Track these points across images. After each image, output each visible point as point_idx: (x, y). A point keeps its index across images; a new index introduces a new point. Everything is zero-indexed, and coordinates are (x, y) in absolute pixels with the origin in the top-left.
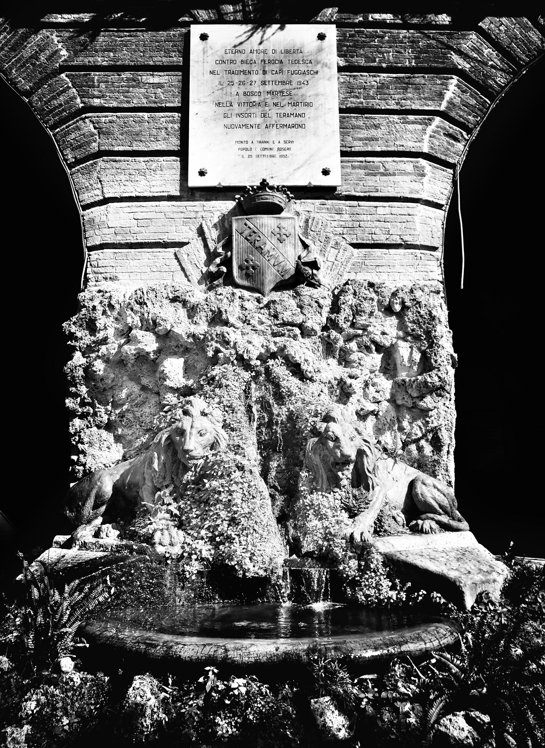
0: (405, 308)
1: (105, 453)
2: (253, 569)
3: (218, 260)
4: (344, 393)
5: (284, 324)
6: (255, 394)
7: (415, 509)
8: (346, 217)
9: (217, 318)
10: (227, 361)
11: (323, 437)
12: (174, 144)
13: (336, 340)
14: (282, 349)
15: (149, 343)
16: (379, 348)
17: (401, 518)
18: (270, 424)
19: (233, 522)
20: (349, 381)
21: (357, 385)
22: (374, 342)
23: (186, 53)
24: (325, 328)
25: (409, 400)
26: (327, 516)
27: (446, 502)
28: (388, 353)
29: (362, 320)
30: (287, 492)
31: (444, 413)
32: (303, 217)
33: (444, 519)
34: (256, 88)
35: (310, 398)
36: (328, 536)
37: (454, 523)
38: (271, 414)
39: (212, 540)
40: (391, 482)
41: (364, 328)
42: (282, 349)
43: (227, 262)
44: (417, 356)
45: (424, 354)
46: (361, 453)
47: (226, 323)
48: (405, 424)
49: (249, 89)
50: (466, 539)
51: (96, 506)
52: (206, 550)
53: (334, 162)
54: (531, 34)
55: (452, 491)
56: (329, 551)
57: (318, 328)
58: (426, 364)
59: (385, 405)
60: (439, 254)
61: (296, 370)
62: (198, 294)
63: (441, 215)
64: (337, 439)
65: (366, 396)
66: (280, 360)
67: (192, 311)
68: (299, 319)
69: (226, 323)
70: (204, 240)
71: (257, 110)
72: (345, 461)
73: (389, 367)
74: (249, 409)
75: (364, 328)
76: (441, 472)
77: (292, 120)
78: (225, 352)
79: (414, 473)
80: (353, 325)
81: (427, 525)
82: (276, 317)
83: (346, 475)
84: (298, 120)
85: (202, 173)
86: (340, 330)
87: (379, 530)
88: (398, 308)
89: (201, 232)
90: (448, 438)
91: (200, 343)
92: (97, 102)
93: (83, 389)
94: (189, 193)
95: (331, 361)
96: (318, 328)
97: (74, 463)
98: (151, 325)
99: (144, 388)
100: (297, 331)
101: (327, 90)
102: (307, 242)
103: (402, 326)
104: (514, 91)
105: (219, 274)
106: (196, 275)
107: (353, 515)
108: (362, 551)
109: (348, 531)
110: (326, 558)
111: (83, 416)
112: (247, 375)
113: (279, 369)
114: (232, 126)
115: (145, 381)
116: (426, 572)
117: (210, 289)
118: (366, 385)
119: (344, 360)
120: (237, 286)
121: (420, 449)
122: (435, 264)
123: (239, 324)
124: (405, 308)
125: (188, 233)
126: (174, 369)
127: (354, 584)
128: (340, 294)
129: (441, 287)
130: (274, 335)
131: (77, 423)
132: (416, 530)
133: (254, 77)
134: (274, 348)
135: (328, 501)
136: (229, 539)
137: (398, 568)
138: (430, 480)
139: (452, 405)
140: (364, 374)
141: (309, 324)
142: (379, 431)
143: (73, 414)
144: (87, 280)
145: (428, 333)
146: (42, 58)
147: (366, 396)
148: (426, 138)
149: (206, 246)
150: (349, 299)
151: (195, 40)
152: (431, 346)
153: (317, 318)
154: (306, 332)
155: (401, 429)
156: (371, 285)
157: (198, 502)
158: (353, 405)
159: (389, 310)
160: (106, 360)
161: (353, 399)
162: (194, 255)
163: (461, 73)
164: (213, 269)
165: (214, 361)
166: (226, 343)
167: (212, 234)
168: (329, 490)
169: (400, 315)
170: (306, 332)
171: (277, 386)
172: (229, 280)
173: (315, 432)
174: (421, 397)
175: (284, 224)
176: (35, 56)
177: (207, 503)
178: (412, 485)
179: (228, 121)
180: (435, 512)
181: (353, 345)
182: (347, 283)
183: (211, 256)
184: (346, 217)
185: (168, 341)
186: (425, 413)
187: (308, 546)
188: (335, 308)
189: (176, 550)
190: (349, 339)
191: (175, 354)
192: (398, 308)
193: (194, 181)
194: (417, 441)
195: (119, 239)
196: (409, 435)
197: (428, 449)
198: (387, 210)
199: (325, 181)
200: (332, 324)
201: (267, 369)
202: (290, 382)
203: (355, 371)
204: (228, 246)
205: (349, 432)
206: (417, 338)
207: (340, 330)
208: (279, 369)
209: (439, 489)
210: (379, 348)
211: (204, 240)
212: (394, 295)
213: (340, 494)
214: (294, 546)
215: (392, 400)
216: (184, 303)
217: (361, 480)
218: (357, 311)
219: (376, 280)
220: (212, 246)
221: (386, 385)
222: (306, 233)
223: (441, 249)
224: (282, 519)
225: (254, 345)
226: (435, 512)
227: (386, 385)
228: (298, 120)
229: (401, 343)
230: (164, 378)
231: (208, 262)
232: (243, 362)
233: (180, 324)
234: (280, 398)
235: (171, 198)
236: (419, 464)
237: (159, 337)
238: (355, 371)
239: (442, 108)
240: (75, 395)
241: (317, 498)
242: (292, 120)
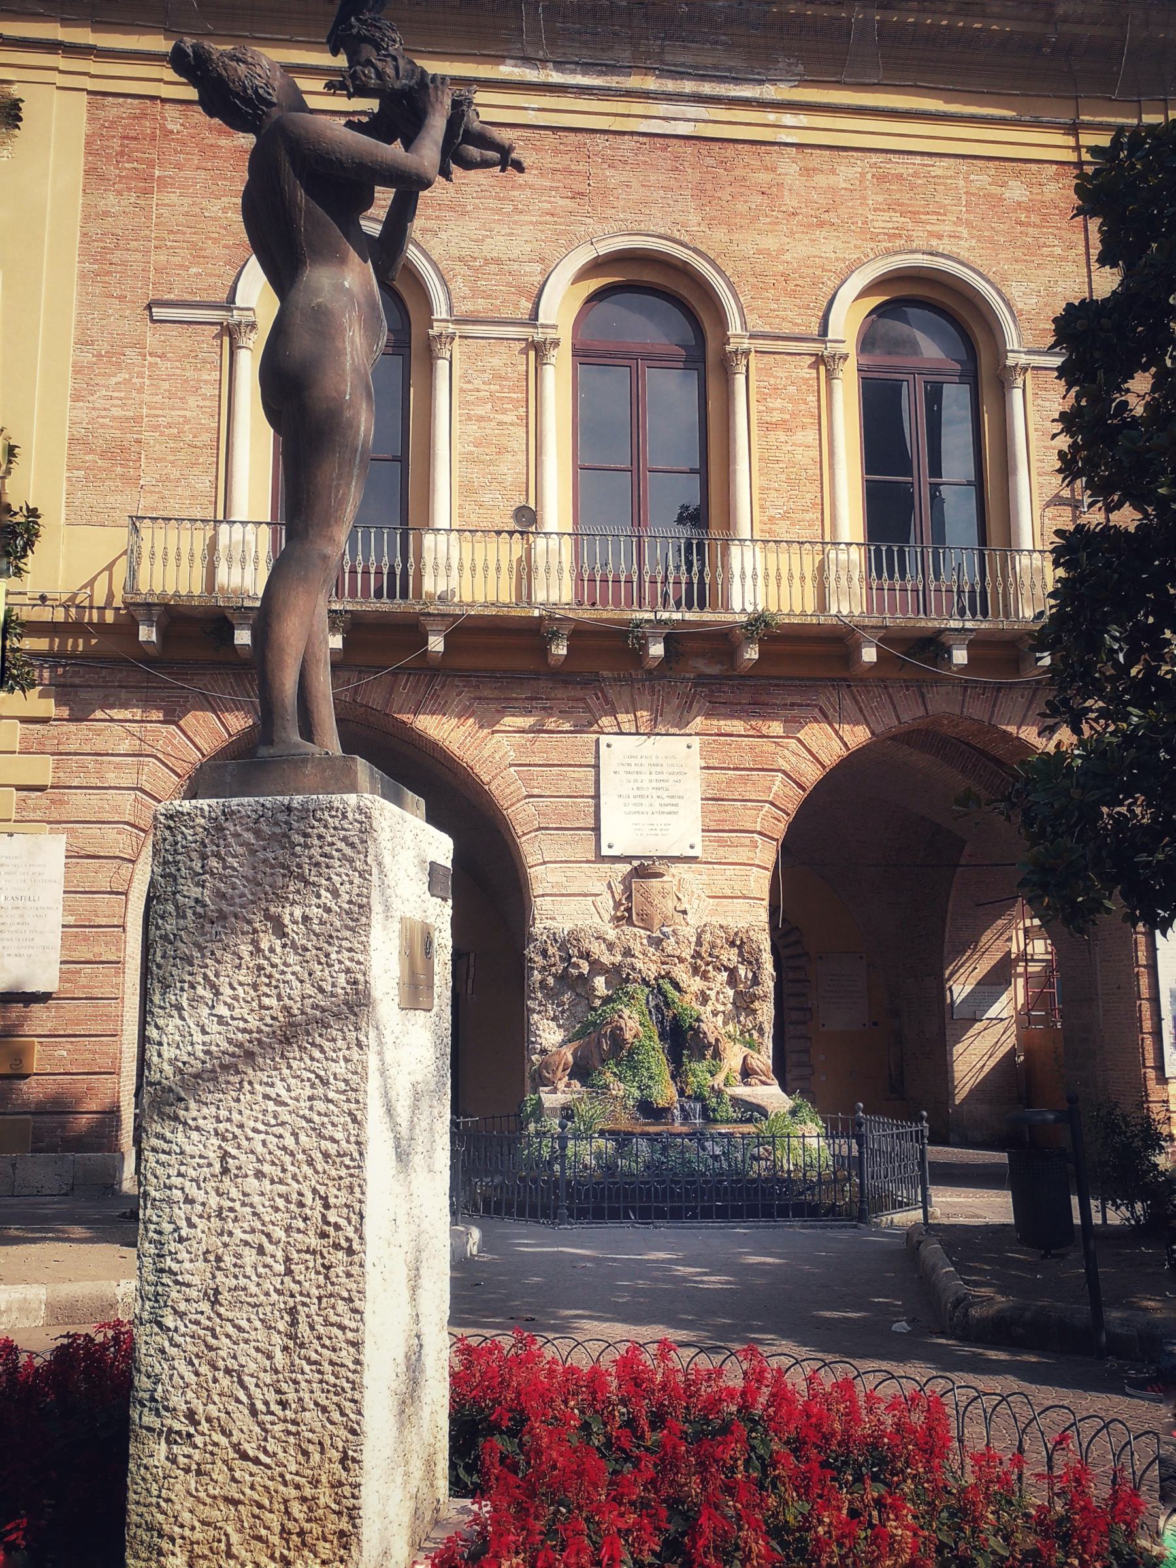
0: (742, 942)
1: (552, 1036)
2: (662, 1103)
3: (622, 908)
4: (704, 999)
5: (668, 956)
6: (652, 1004)
7: (747, 1073)
8: (704, 877)
9: (628, 953)
10: (635, 981)
11: (697, 1031)
12: (591, 823)
13: (700, 966)
14: (668, 973)
15: (585, 967)
16: (726, 969)
17: (739, 1078)
18: (662, 1022)
19: (651, 1078)
20: (708, 992)
21: (712, 994)
22: (723, 965)
23: (597, 757)
24: (693, 957)
25: (744, 1003)
26: (698, 1071)
27: (764, 1068)
28: (732, 972)
29: (716, 952)
30: (675, 1059)
31: (766, 1012)
32: (677, 878)
33: (763, 1078)
34: (644, 785)
35: (688, 1003)
36: (700, 1086)
37: (769, 1081)
38: (663, 1014)
39: (639, 1088)
40: (734, 1056)
41: (717, 957)
42: (668, 973)
43: (629, 910)
44: (750, 975)
45: (754, 973)
46: (717, 1040)
47: (633, 956)
48: (742, 1019)
49: (639, 785)
50: (775, 1089)
51: (564, 1070)
52: (637, 1094)
53: (697, 838)
54: (833, 742)
55: (770, 1062)
56: (701, 1094)
57: (688, 957)
58: (756, 981)
59: (730, 1006)
60: (766, 903)
61: (676, 986)
62: (612, 934)
63: (769, 874)
64: (705, 1033)
65: (717, 1000)
66: (667, 980)
67: (610, 946)
68: (677, 953)
69: (633, 956)
70: (612, 892)
71: (645, 801)
72: (710, 1044)
73: (733, 980)
74: (650, 1012)
75: (717, 957)
76: (763, 1050)
77: (669, 809)
78: (633, 975)
79: (747, 1050)
80: (710, 955)
81: (753, 1082)
82: (663, 951)
83: (709, 1053)
84: (674, 809)
85: (610, 847)
86: (702, 959)
87: (727, 1083)
88: (738, 943)
89: (610, 887)
90: (769, 1029)
91: (617, 968)
92: (536, 791)
93: (539, 995)
94: (601, 859)
95: (697, 978)
96: (688, 957)
97: (533, 1043)
98: (586, 956)
99: (578, 995)
100: (677, 961)
101: (692, 787)
102: (680, 896)
103: (740, 954)
104: (820, 786)
105: (623, 917)
106: (607, 917)
107: (713, 1075)
108: (719, 1094)
109: (711, 1084)
110: (699, 1098)
111: (539, 1012)
112: (647, 990)
113: (667, 987)
114: (629, 813)
115: (579, 991)
116: (751, 1104)
117: (617, 927)
118: (718, 993)
119: (705, 976)
120: (635, 926)
121: (751, 1035)
122: (763, 910)
123: (641, 956)
124: (742, 942)
125: (600, 887)
126: (600, 982)
127: (714, 1110)
128: (703, 931)
129: (767, 926)
130: (663, 963)
131: (535, 1016)
132: (746, 1084)
133: (643, 777)
134: (663, 973)
135: (700, 1067)
136: (649, 1087)
137: (736, 1101)
138: (756, 1055)
139: (772, 1006)
140: (717, 987)
141: (683, 955)
142: (725, 1023)
143: (533, 1011)
144: (534, 919)
145: (757, 960)
146: (497, 756)
147: (717, 1000)
148: (759, 820)
149: (613, 897)
150: (707, 937)
151: (603, 747)
152: (759, 968)
153: (688, 950)
154: (681, 960)
155: (739, 1022)
156: (721, 927)
157: (630, 1068)
158: (709, 1008)
159: (732, 944)
160: (554, 976)
161: (710, 1003)
162: (607, 903)
163: (785, 773)
164: (619, 914)
165: (627, 980)
166: (634, 969)
167: (619, 888)
168: (699, 1061)
169: (740, 947)
170: (681, 960)
171: (666, 997)
172: (630, 922)
173: (691, 1027)
174: (752, 1002)
175: (666, 886)
176: (492, 756)
177: (635, 1068)
178: (745, 1058)
179: (627, 809)
180: (757, 1074)
181: (710, 968)
182: (705, 926)
183: (617, 905)
184: (704, 877)
185: (597, 967)
186: (754, 1011)
187: (689, 1092)
188: (699, 943)
189: (621, 1093)
190: (708, 964)
191: (599, 974)
192: (738, 943)
193: (605, 851)
194: (749, 1031)
195: (555, 891)
196: (744, 1026)
197: (756, 1035)
198: (732, 872)
199: (692, 853)
200: (697, 955)
201: (659, 985)
202: (673, 994)
203: (712, 985)
204: (629, 898)
205: (713, 1025)
206: (750, 963)
207: (702, 959)
208: (667, 987)
209: (764, 1059)
210: (726, 969)
211: (612, 892)
212: (736, 934)
213: (706, 1063)
214: (681, 1093)
215: (734, 1003)
216: (604, 940)
217: (717, 1055)
218: (713, 946)
219: (724, 923)
220: (617, 898)
221: (731, 993)
222: (679, 890)
223: (768, 899)
224: (673, 1077)
225: (650, 970)
226: (757, 1074)
227: (731, 993)
228: (674, 809)
229: (740, 966)
230: (594, 989)
231: (616, 908)
232: (646, 983)
233: (606, 959)
234: (667, 1005)
235: (588, 862)
236: (750, 1045)
237: (590, 964)
238: (712, 985)
239: (770, 799)
240: (535, 999)
241: (694, 1065)
242: (669, 809)
